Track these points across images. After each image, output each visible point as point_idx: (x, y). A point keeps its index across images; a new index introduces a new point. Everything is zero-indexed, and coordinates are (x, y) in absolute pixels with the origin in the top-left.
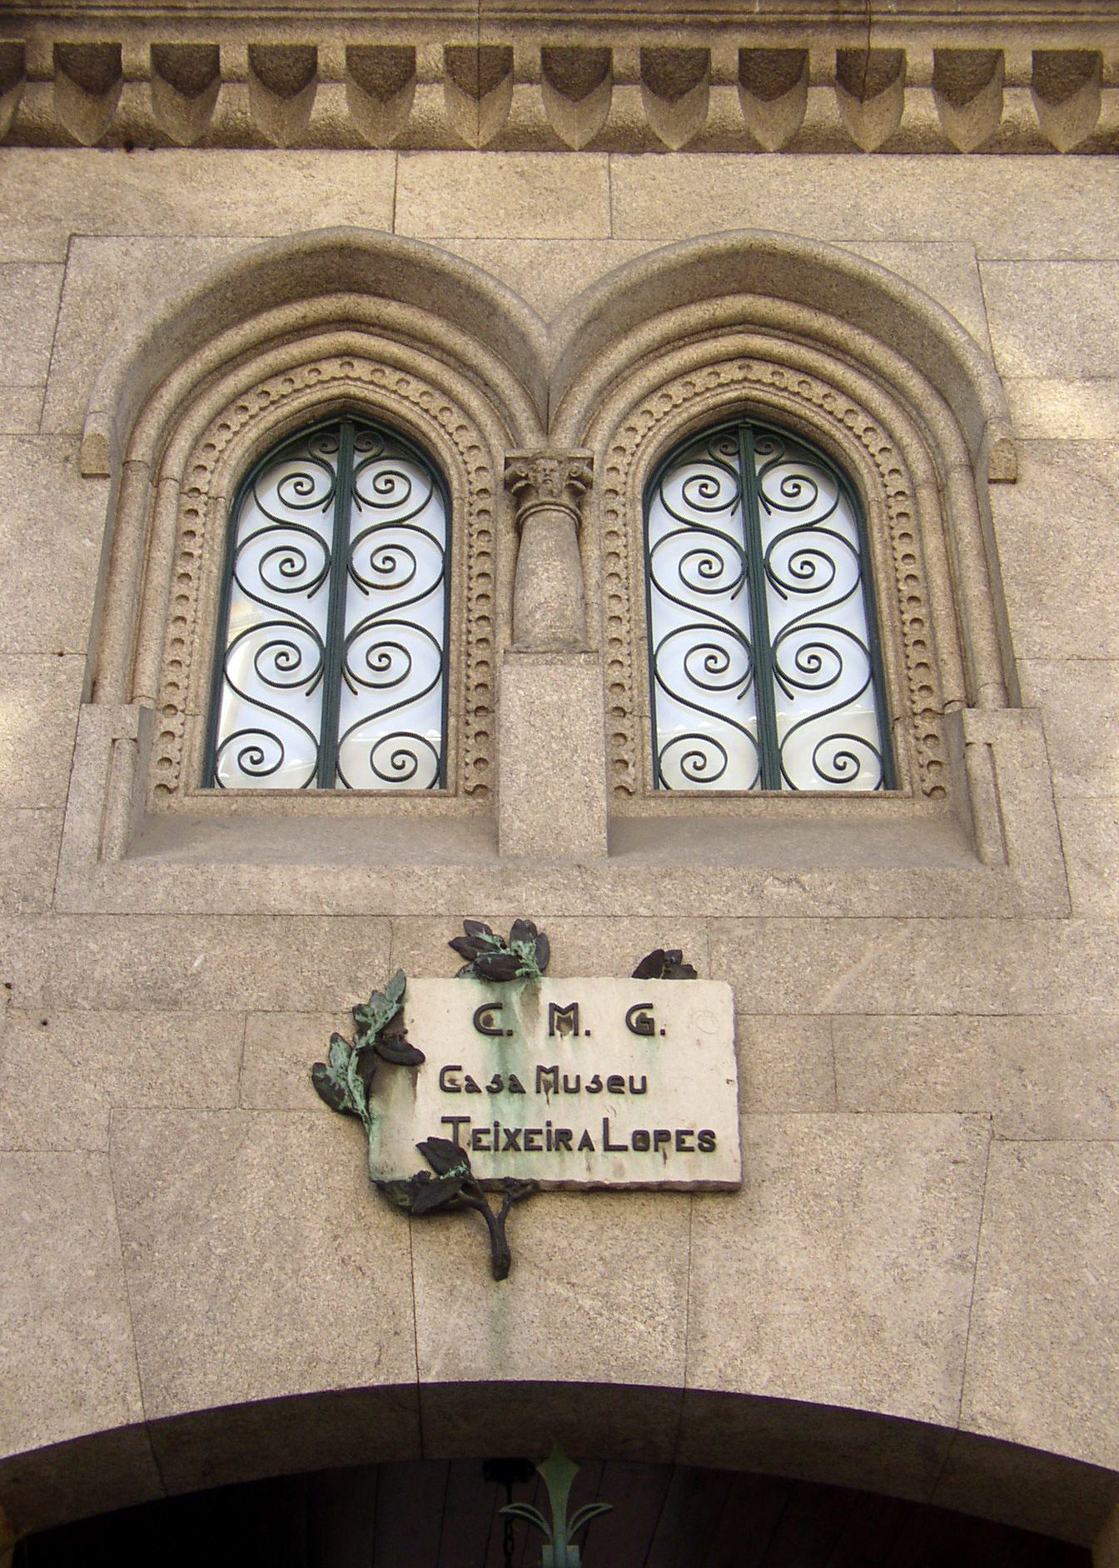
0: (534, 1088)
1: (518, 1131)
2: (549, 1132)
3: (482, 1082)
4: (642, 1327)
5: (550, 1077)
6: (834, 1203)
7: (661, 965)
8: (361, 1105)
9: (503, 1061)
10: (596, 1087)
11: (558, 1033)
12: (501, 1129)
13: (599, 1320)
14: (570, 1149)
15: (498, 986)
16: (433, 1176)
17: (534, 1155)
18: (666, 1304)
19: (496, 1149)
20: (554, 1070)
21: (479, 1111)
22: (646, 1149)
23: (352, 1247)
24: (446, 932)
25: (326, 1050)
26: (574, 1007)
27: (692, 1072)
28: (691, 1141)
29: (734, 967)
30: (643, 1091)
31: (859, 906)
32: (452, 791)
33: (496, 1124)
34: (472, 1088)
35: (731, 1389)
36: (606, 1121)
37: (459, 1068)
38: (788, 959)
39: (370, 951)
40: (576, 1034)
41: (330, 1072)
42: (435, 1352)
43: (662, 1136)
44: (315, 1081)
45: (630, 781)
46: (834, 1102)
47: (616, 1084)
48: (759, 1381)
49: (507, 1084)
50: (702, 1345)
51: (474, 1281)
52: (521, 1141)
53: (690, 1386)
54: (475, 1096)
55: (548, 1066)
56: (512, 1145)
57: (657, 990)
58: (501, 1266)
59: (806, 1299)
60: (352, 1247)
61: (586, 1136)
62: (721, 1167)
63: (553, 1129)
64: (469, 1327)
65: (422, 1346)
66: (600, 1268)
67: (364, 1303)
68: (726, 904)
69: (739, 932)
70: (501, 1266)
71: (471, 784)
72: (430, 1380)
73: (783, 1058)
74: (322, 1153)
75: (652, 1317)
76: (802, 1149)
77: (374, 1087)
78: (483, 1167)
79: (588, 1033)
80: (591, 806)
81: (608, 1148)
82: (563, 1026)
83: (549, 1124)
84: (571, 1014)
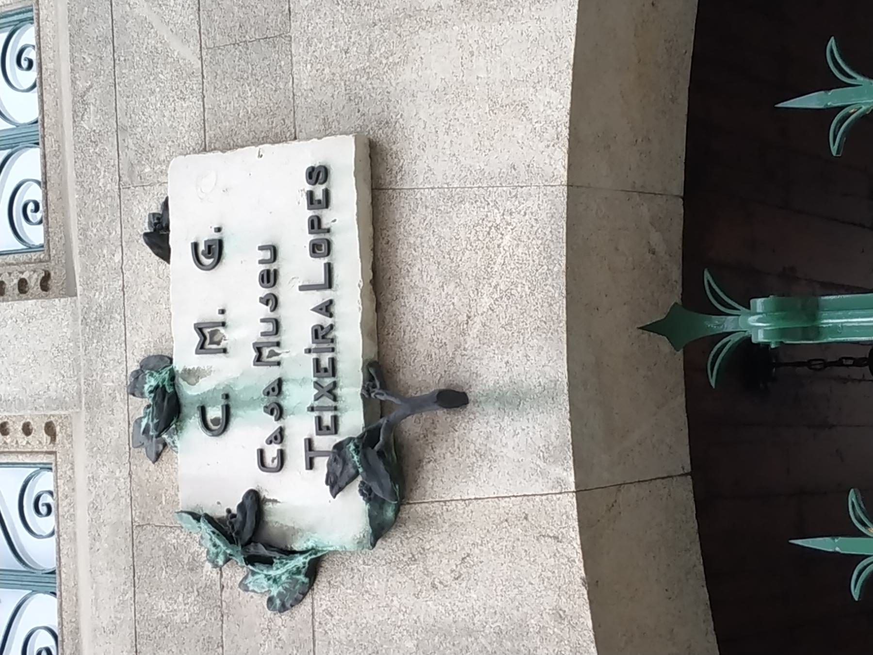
0: (276, 368)
1: (317, 385)
2: (317, 351)
3: (271, 425)
4: (507, 237)
5: (266, 352)
6: (377, 30)
7: (158, 238)
8: (300, 561)
9: (250, 403)
10: (272, 301)
11: (223, 344)
12: (316, 404)
13: (502, 287)
14: (332, 327)
15: (185, 410)
16: (360, 479)
17: (340, 366)
18: (483, 213)
19: (336, 409)
20: (259, 350)
21: (300, 427)
22: (329, 243)
23: (443, 570)
24: (145, 467)
25: (255, 596)
26: (200, 329)
27: (249, 194)
28: (319, 194)
29: (162, 158)
30: (274, 251)
31: (104, 28)
32: (53, 457)
33: (312, 409)
34: (279, 436)
35: (566, 132)
36: (302, 288)
37: (261, 453)
38: (152, 99)
39: (165, 548)
40: (223, 324)
41: (275, 591)
42: (543, 474)
43: (315, 224)
44: (283, 608)
45: (35, 276)
46: (279, 38)
47: (269, 278)
48: (555, 102)
49: (273, 398)
50: (522, 169)
51: (477, 428)
52: (327, 381)
53: (565, 180)
54: (287, 433)
55: (254, 354)
56: (331, 392)
57: (179, 241)
58: (454, 399)
59: (472, 54)
60: (443, 570)
61: (318, 309)
62: (341, 155)
63: (314, 346)
64: (516, 434)
65: (538, 489)
66: (450, 288)
67: (497, 554)
68: (107, 170)
69: (131, 154)
70: (454, 399)
71: (46, 438)
72: (572, 479)
73: (243, 97)
74: (353, 601)
75: (497, 228)
76: (327, 70)
77: (283, 546)
78: (353, 422)
79: (223, 312)
80: (32, 318)
81: (329, 283)
82: (216, 339)
83: (309, 351)
84: (207, 331)
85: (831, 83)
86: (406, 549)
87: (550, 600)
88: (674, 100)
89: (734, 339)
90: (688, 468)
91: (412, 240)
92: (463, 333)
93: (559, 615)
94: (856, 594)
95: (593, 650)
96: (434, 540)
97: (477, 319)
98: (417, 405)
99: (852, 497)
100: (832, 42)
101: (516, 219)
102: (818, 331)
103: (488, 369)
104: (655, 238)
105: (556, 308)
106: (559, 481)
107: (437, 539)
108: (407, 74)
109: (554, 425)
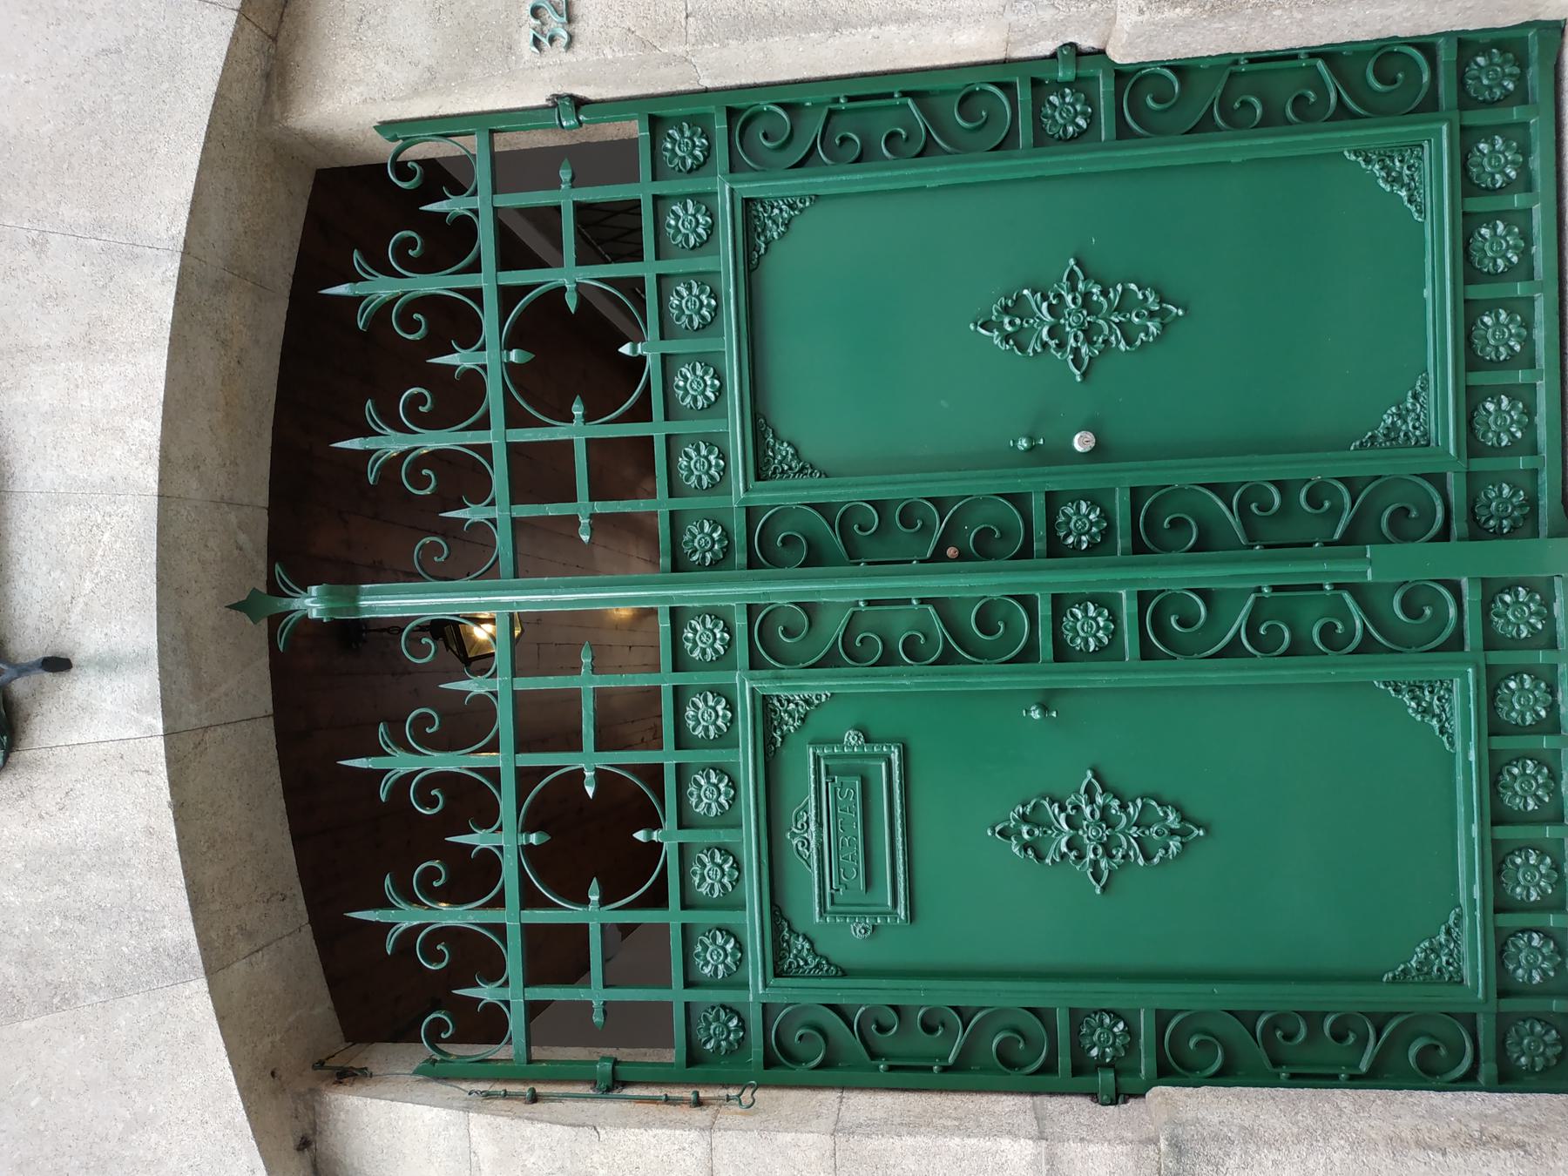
4: (107, 535)
18: (85, 514)
35: (157, 454)
42: (137, 722)
48: (149, 429)
50: (120, 480)
51: (76, 687)
53: (156, 491)
58: (58, 664)
65: (132, 733)
66: (56, 574)
70: (58, 664)
85: (368, 432)
86: (15, 788)
87: (141, 821)
88: (259, 435)
89: (297, 615)
90: (271, 711)
91: (22, 534)
92: (68, 611)
93: (149, 832)
94: (383, 797)
95: (1563, 1097)
96: (41, 779)
97: (81, 600)
98: (24, 670)
99: (381, 728)
100: (369, 403)
101: (115, 519)
102: (358, 609)
103: (87, 640)
104: (242, 538)
105: (148, 591)
106: (151, 727)
107: (43, 778)
108: (19, 399)
109: (146, 683)
